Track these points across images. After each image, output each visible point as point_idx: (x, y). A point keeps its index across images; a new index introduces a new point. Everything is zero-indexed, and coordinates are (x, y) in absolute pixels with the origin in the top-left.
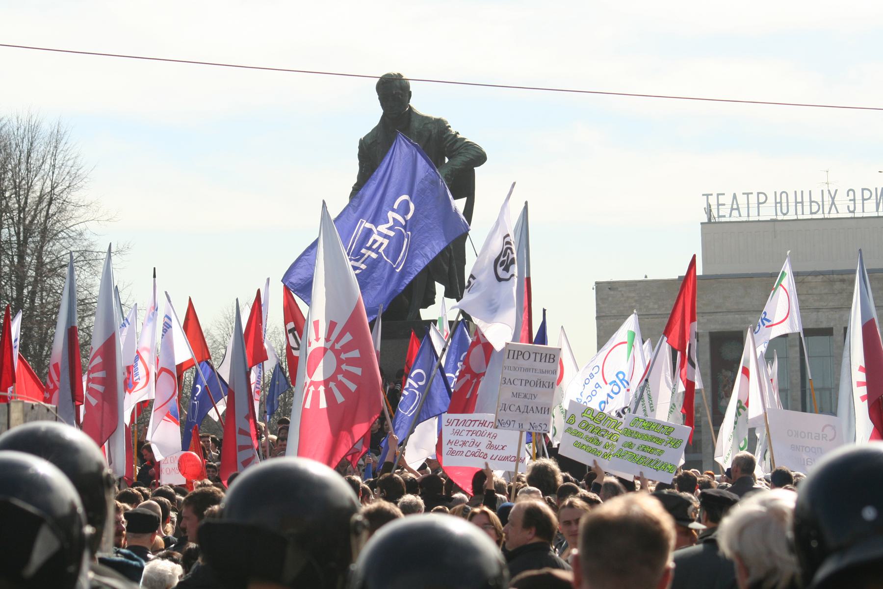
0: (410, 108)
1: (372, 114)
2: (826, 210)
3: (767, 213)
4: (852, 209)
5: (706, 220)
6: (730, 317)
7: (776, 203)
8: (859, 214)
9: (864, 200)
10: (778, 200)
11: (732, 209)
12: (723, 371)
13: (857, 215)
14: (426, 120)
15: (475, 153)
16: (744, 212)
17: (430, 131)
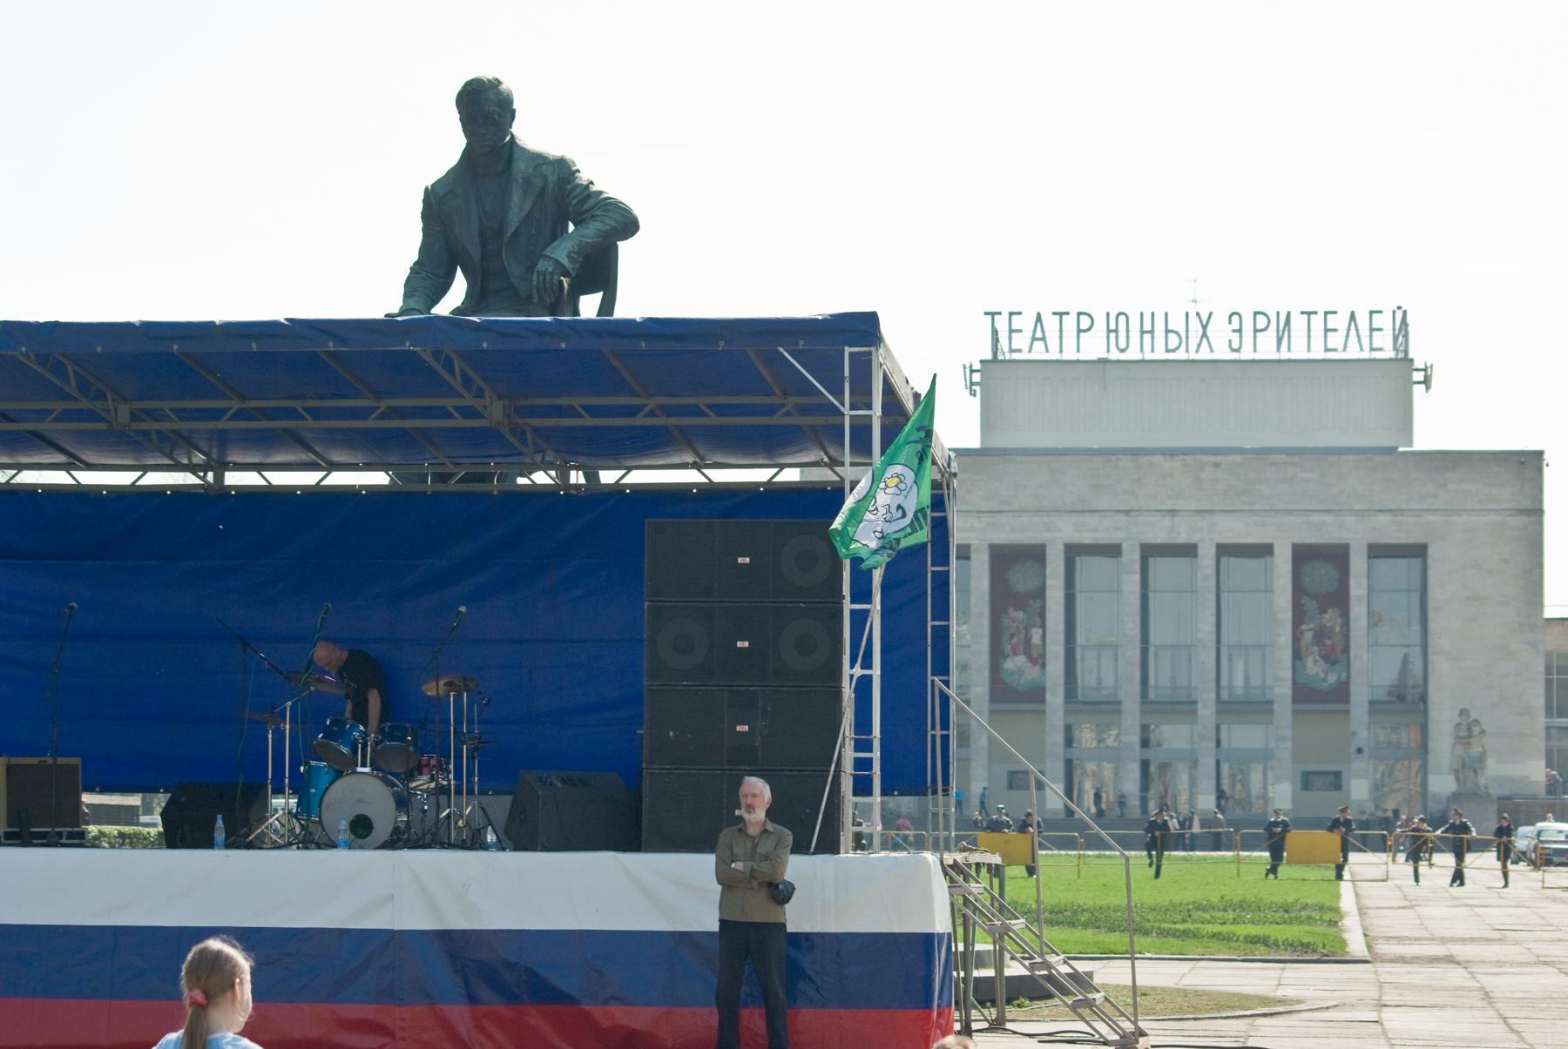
0: (427, 279)
1: (446, 145)
2: (1192, 347)
3: (1094, 347)
4: (1235, 346)
5: (989, 356)
6: (1025, 519)
7: (1109, 331)
8: (1247, 354)
9: (1256, 331)
10: (1112, 327)
11: (1034, 339)
12: (1011, 610)
14: (539, 160)
15: (617, 217)
17: (545, 177)
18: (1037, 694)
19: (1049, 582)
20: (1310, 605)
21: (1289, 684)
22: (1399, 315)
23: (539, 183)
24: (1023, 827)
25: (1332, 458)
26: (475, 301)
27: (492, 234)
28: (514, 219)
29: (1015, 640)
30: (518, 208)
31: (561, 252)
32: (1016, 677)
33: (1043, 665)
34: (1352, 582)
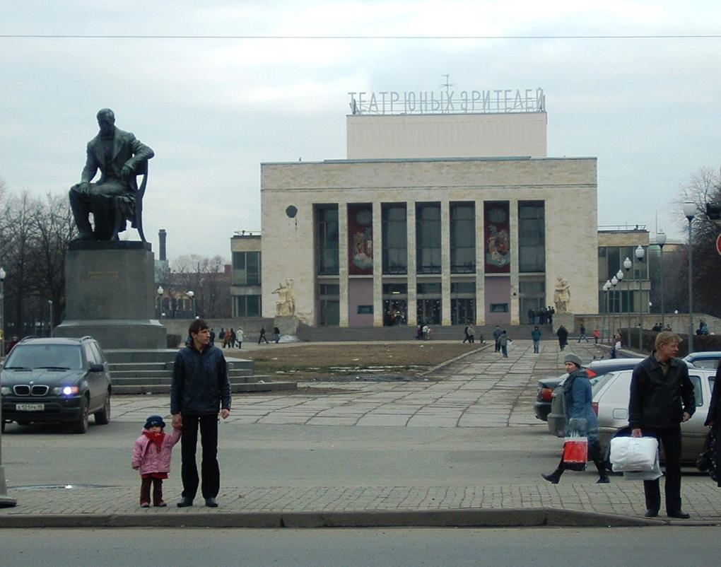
0: (90, 171)
1: (95, 130)
3: (399, 108)
11: (371, 105)
13: (468, 112)
14: (123, 134)
16: (380, 107)
17: (124, 140)
18: (369, 270)
19: (374, 220)
20: (493, 229)
21: (483, 264)
22: (539, 92)
23: (123, 142)
25: (501, 162)
26: (105, 179)
27: (108, 157)
28: (115, 154)
29: (360, 246)
31: (130, 164)
32: (360, 263)
33: (372, 258)
34: (511, 218)
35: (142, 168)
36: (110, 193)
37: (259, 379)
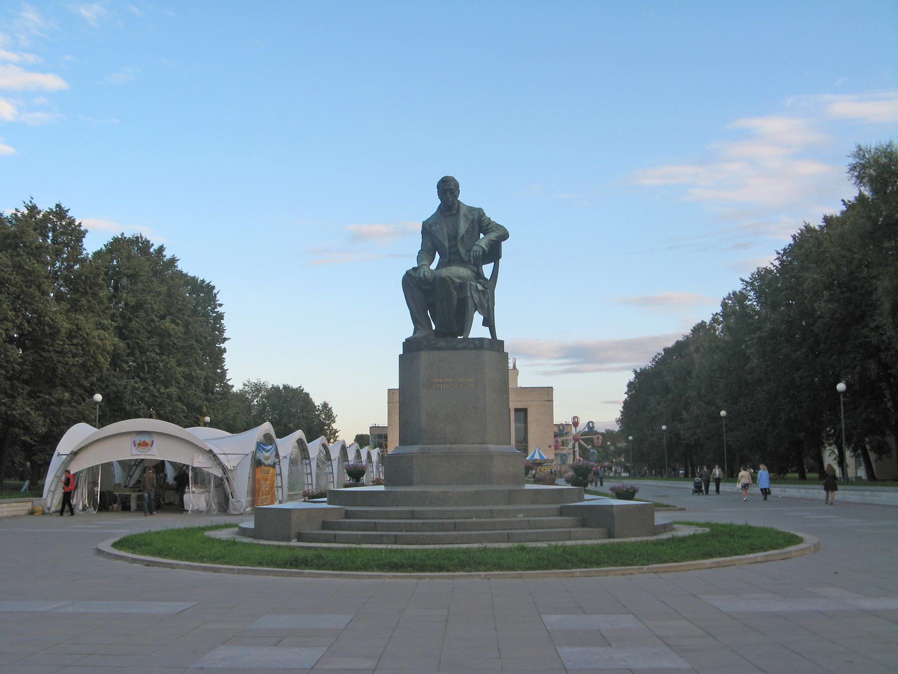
0: (426, 253)
1: (433, 204)
14: (471, 209)
24: (496, 629)
30: (463, 227)
35: (493, 254)
36: (459, 278)
37: (519, 511)
